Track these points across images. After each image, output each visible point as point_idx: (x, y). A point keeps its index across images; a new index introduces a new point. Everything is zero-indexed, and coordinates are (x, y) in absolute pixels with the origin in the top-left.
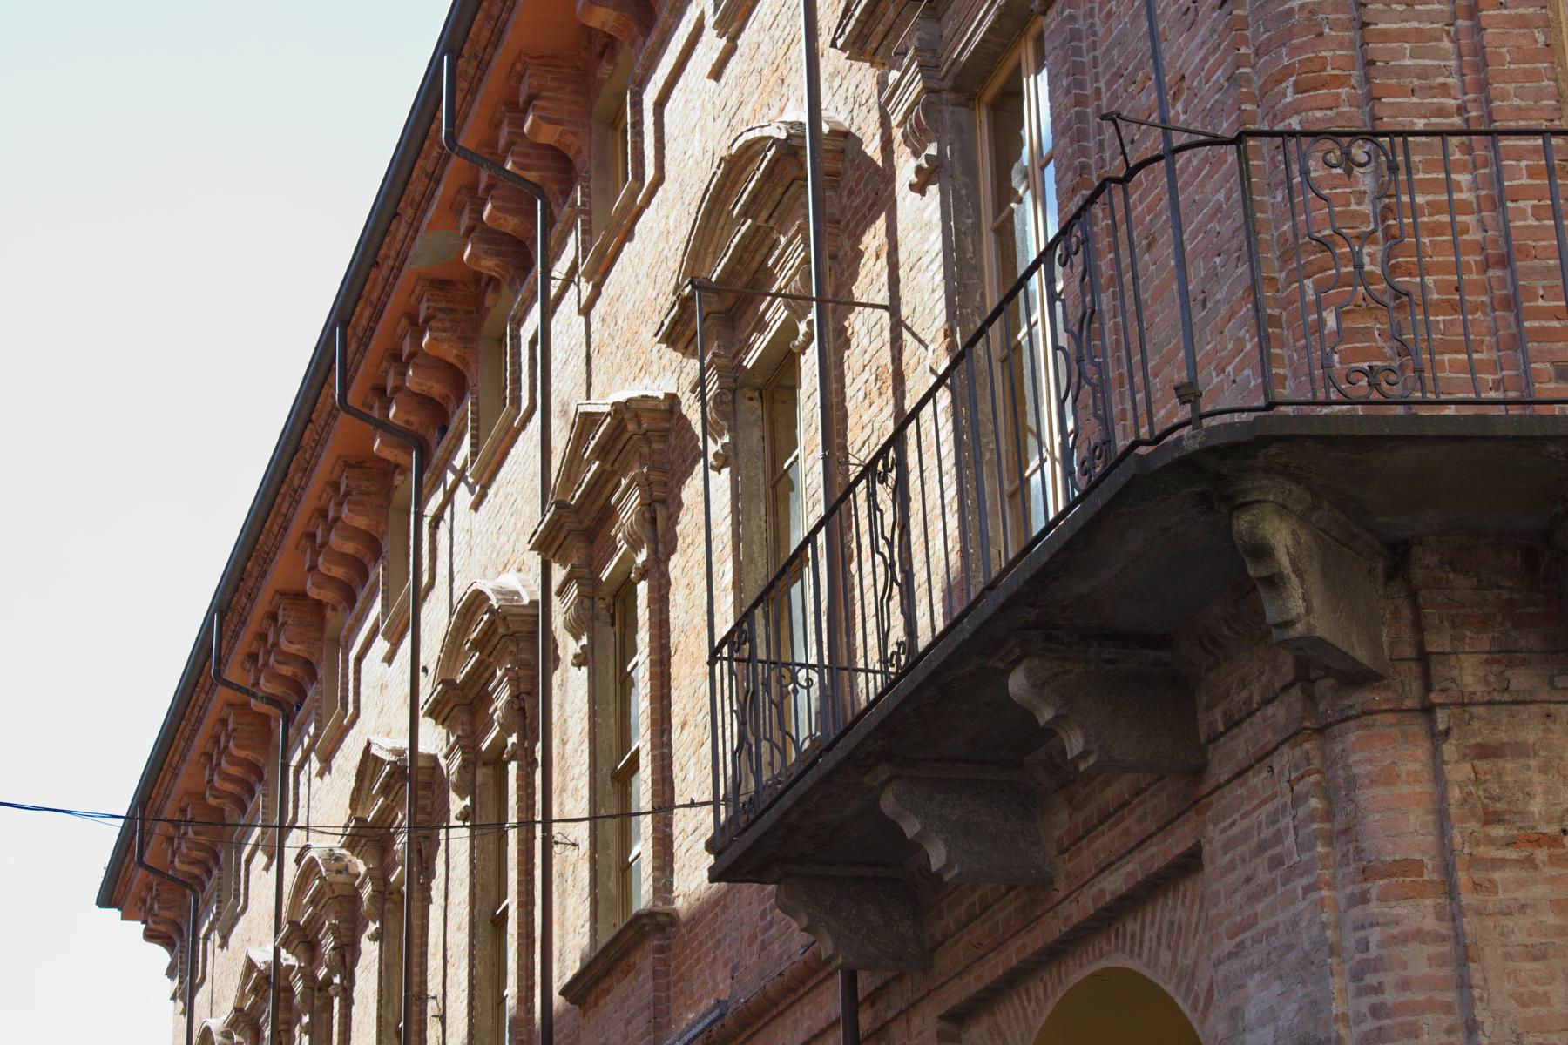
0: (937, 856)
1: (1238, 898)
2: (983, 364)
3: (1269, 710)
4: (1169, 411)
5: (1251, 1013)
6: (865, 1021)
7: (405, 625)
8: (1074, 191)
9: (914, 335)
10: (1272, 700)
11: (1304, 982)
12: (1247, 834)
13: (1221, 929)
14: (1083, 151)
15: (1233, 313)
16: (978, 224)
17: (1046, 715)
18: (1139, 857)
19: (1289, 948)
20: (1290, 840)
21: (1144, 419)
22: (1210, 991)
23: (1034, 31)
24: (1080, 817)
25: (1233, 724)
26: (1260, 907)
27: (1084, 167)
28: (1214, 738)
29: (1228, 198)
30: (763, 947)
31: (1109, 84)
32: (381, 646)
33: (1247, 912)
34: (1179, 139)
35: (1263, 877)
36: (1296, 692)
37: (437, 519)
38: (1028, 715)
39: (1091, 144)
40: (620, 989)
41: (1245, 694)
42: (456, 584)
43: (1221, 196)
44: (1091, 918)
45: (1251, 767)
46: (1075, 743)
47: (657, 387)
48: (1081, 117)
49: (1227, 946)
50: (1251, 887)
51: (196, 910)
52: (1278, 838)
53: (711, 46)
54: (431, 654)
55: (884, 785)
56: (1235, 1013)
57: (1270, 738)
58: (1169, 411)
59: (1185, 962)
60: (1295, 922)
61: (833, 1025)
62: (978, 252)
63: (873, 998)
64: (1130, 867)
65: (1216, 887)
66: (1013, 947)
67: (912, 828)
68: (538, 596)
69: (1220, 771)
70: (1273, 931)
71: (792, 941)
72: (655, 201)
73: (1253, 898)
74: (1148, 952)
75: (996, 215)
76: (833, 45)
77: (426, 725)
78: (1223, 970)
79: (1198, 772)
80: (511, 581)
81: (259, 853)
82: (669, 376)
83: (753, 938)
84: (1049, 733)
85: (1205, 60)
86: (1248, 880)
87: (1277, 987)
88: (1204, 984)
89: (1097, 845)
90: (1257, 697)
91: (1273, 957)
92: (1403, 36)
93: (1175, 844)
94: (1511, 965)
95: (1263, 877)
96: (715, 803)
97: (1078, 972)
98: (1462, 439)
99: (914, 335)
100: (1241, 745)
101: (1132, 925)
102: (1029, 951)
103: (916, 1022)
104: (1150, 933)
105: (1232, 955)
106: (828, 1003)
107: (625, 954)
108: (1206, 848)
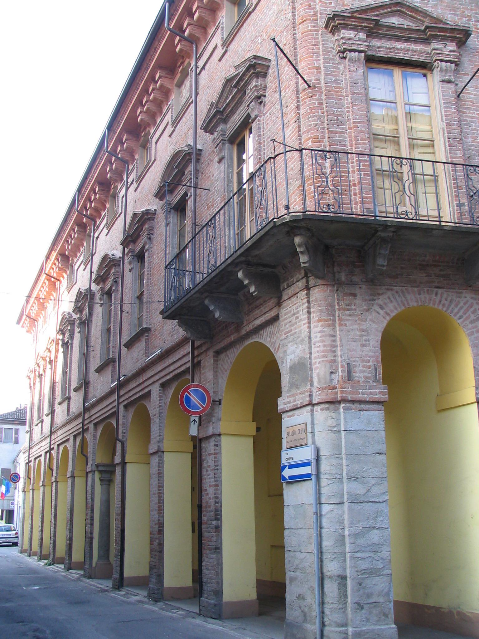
0: (217, 315)
1: (287, 326)
2: (232, 203)
3: (298, 283)
4: (283, 211)
5: (289, 352)
6: (196, 353)
7: (89, 261)
8: (257, 163)
9: (42, 427)
10: (298, 281)
11: (302, 345)
12: (290, 311)
13: (283, 333)
14: (260, 155)
15: (294, 193)
16: (233, 171)
17: (246, 282)
18: (264, 316)
19: (299, 337)
20: (301, 313)
21: (276, 213)
22: (279, 347)
23: (249, 127)
24: (250, 307)
25: (289, 286)
26: (292, 328)
27: (260, 158)
28: (284, 289)
29: (294, 166)
30: (172, 336)
31: (267, 140)
32: (83, 267)
33: (289, 329)
34: (288, 149)
35: (294, 321)
36: (304, 280)
37: (98, 237)
38: (242, 282)
39: (262, 153)
40: (137, 345)
41: (292, 280)
42: (193, 112)
43: (293, 166)
44: (252, 330)
45: (292, 296)
46: (252, 289)
47: (152, 208)
48: (260, 147)
49: (284, 337)
50: (291, 323)
51: (94, 230)
52: (298, 312)
53: (169, 129)
54: (95, 268)
55: (206, 297)
56: (285, 352)
57: (298, 290)
58: (283, 211)
59: (273, 340)
60: (301, 331)
61: (188, 353)
62: (232, 178)
63: (198, 347)
64: (262, 319)
65: (282, 323)
66: (232, 336)
67: (212, 308)
68: (121, 256)
69: (285, 297)
70: (295, 333)
71: (180, 333)
72: (154, 165)
73: (291, 326)
74: (266, 339)
75: (238, 167)
76: (201, 129)
77: (93, 284)
78: (283, 342)
79: (280, 297)
80: (114, 252)
81: (82, 265)
82: (154, 205)
83: (169, 334)
84: (246, 286)
85: (290, 135)
86: (290, 322)
87: (295, 346)
88: (278, 345)
89: (254, 313)
90: (295, 280)
91: (295, 339)
92: (336, 132)
93: (273, 313)
94: (349, 343)
95: (294, 321)
96: (165, 302)
97: (247, 343)
98: (347, 222)
99: (42, 427)
100: (290, 291)
101: (261, 332)
102: (236, 337)
103: (208, 353)
104: (265, 334)
105: (285, 338)
106: (188, 348)
107: (139, 337)
108: (280, 315)
